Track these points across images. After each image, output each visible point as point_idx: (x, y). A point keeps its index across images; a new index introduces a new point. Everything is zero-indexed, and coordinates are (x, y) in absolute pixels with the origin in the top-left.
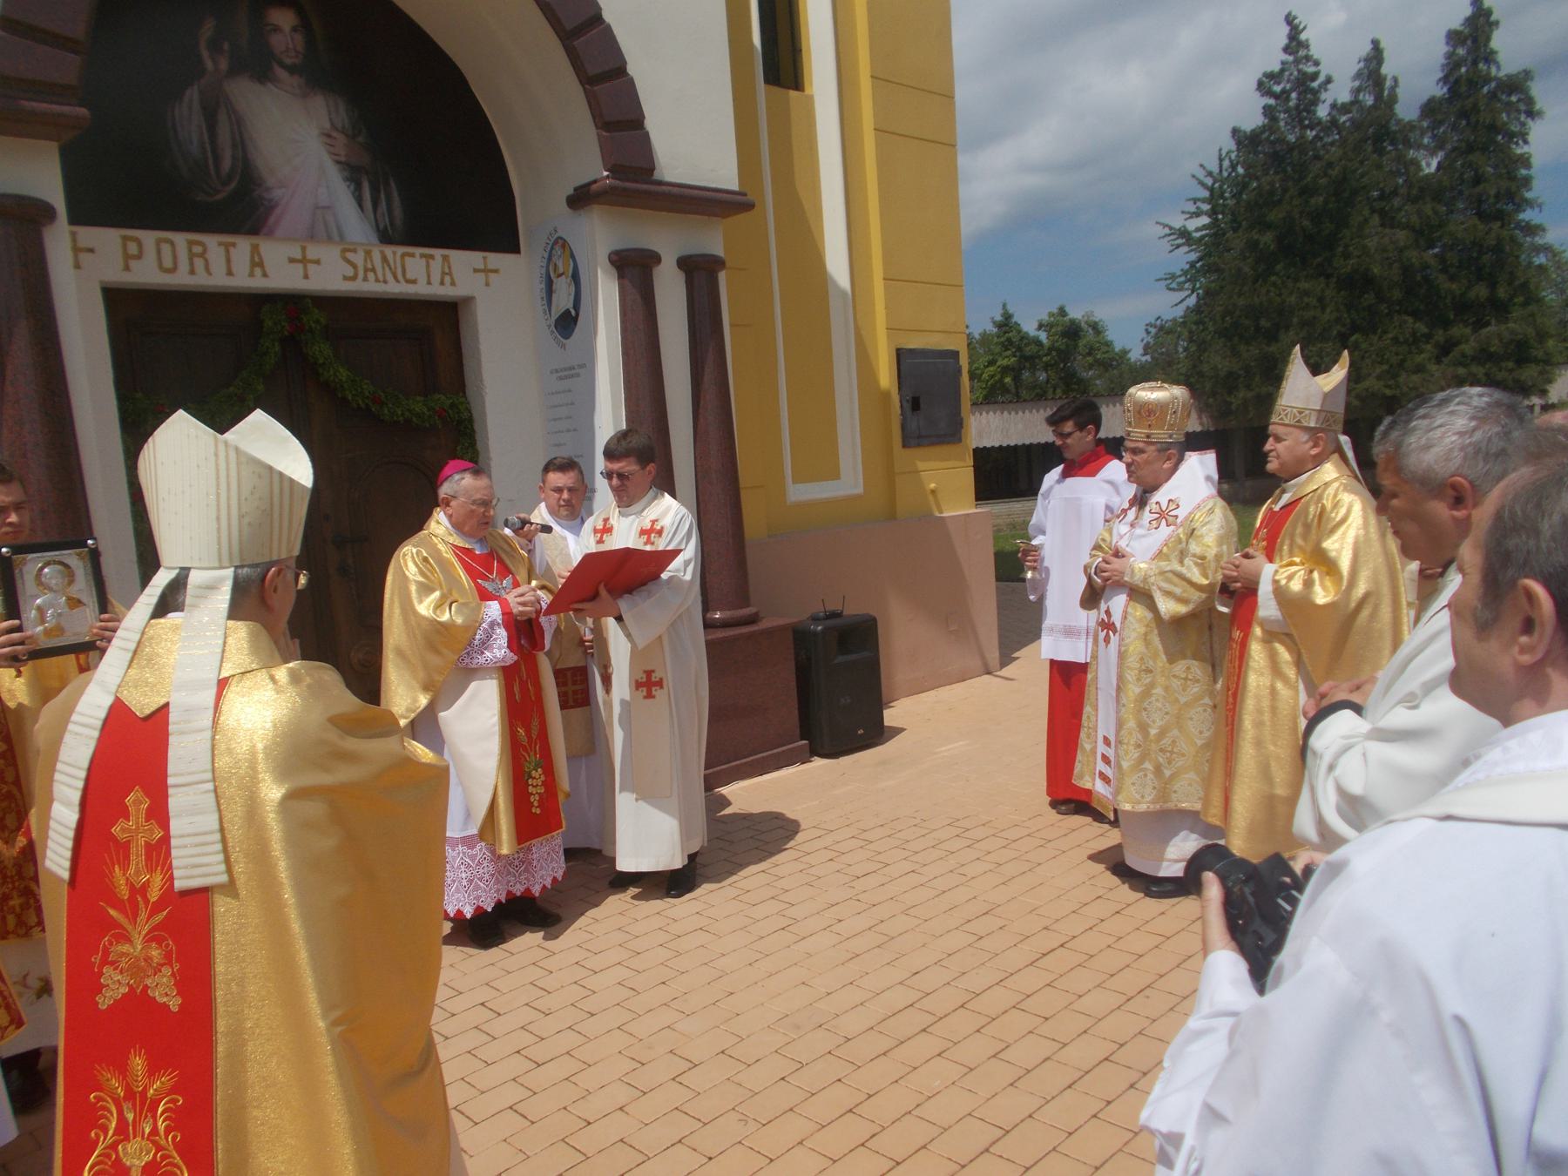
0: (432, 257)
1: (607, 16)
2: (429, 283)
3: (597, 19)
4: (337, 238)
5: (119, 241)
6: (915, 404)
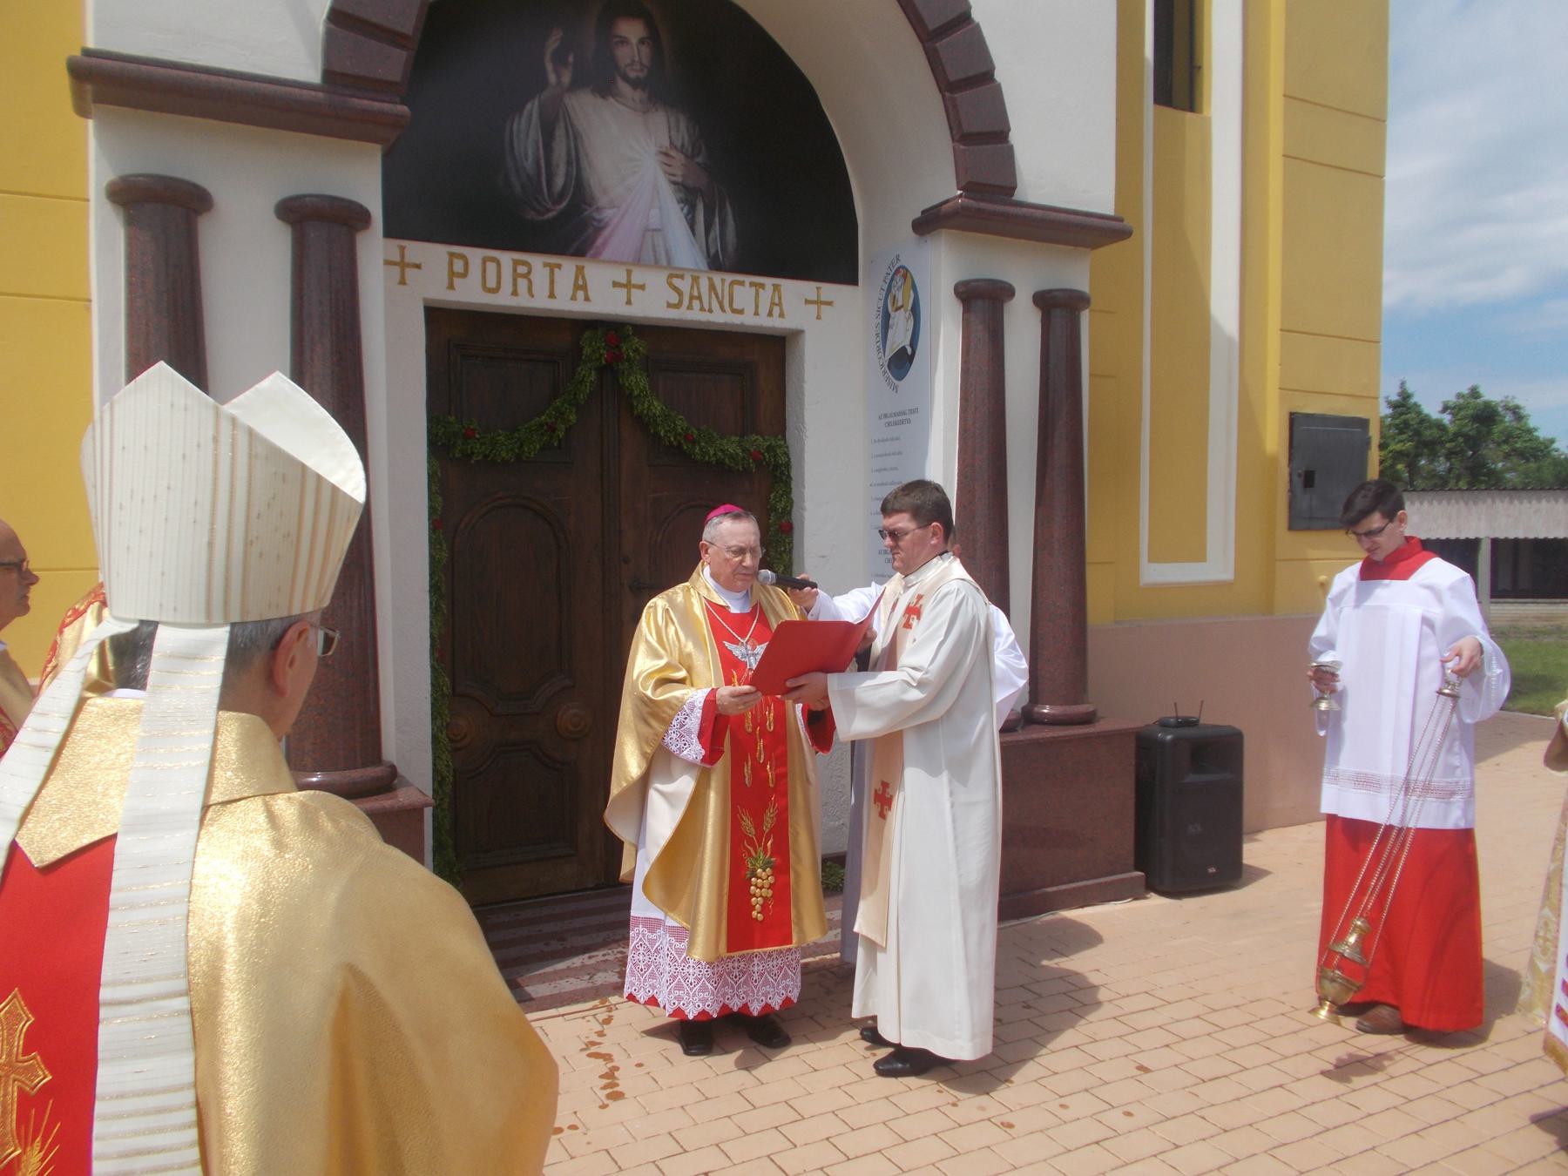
0: (762, 286)
1: (976, 15)
2: (756, 313)
3: (965, 18)
4: (664, 262)
5: (446, 258)
6: (1308, 480)
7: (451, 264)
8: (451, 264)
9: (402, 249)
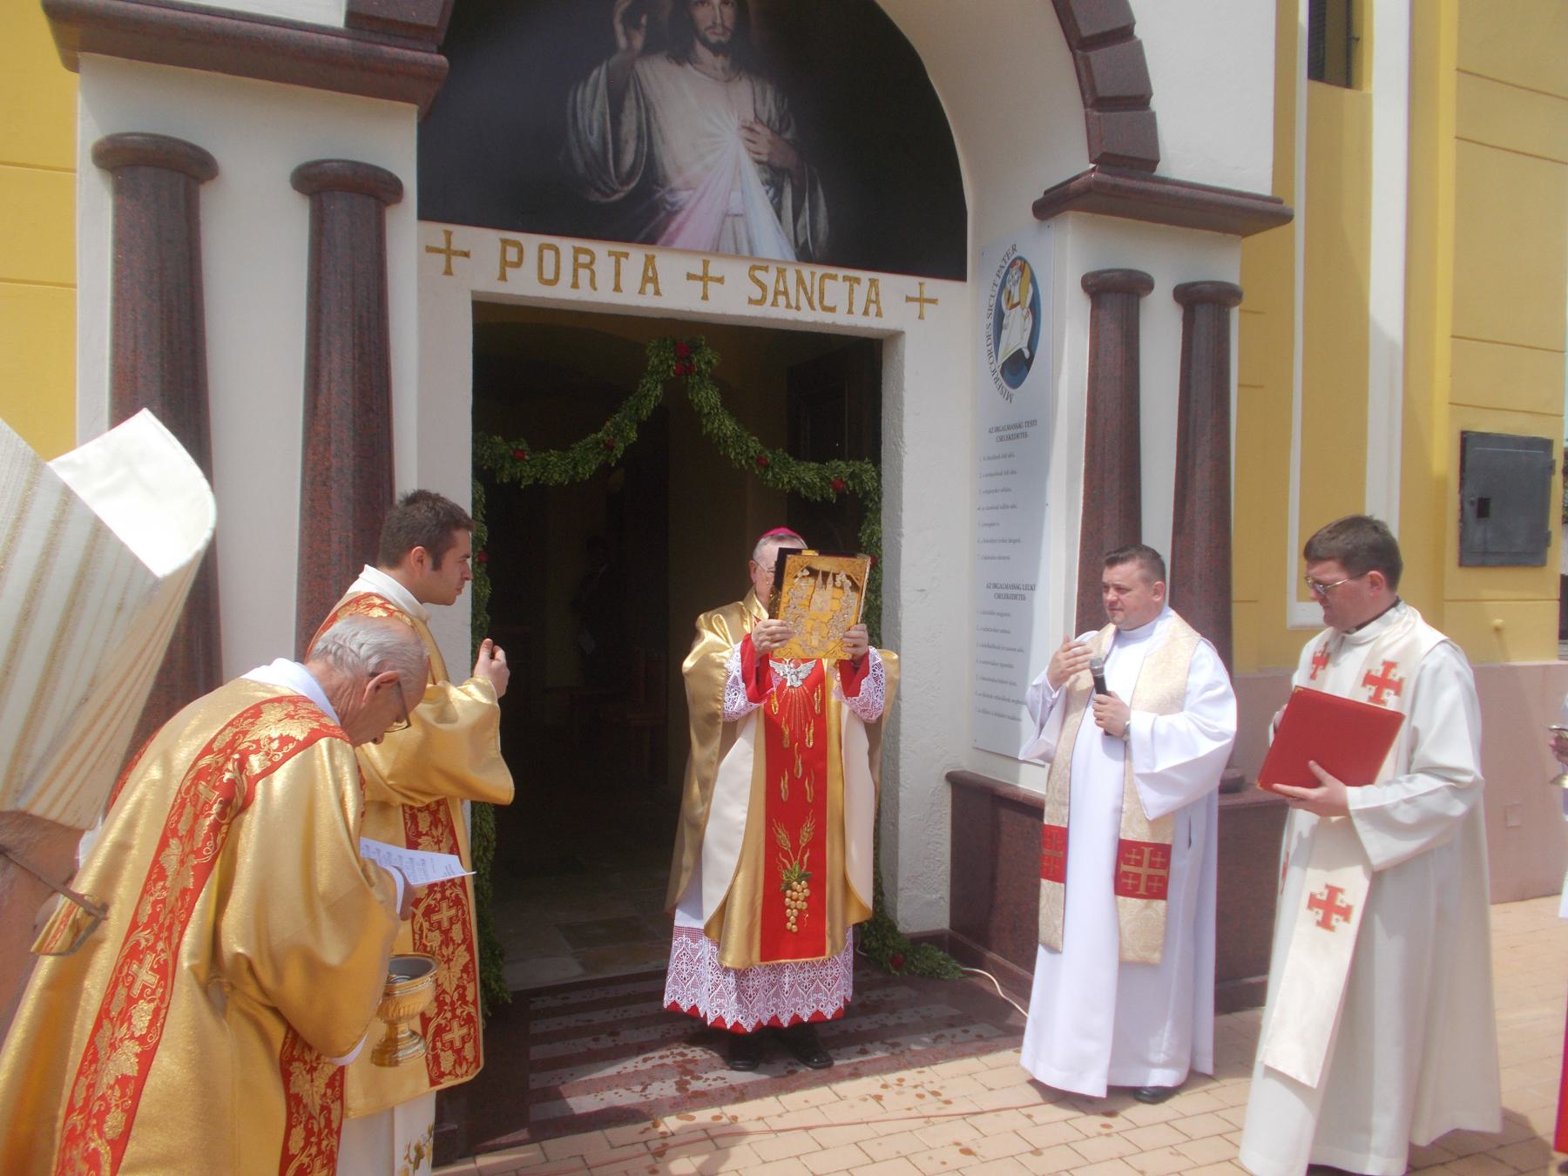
0: (857, 280)
2: (850, 312)
4: (746, 252)
7: (504, 252)
8: (504, 252)
9: (449, 234)
